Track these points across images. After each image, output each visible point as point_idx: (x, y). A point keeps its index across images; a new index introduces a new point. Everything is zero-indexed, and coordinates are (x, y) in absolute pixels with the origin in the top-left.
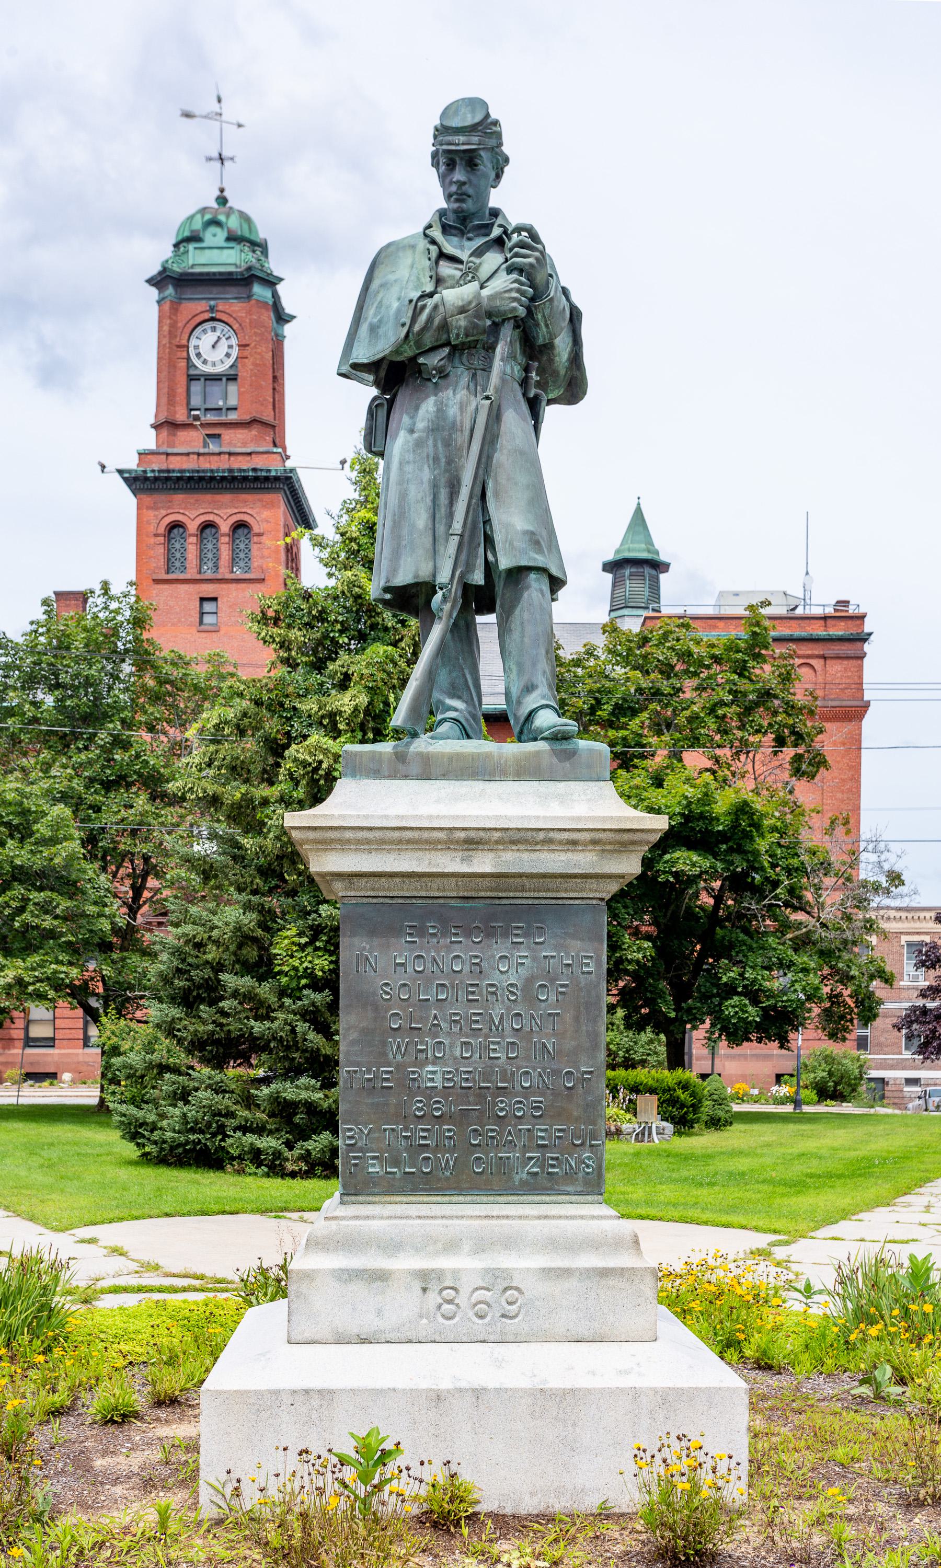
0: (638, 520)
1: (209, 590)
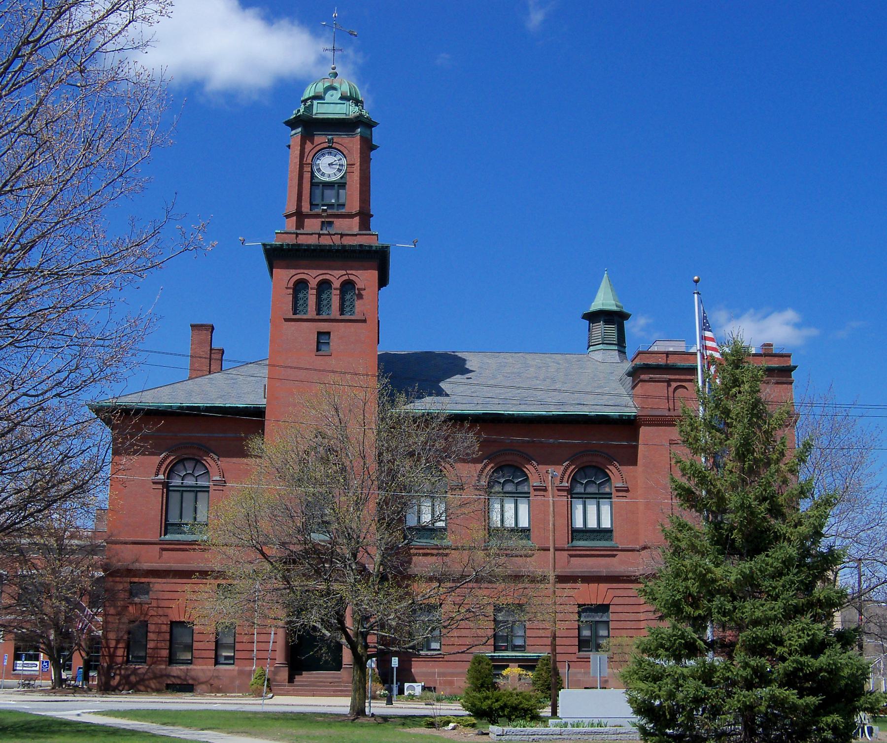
1: (324, 327)
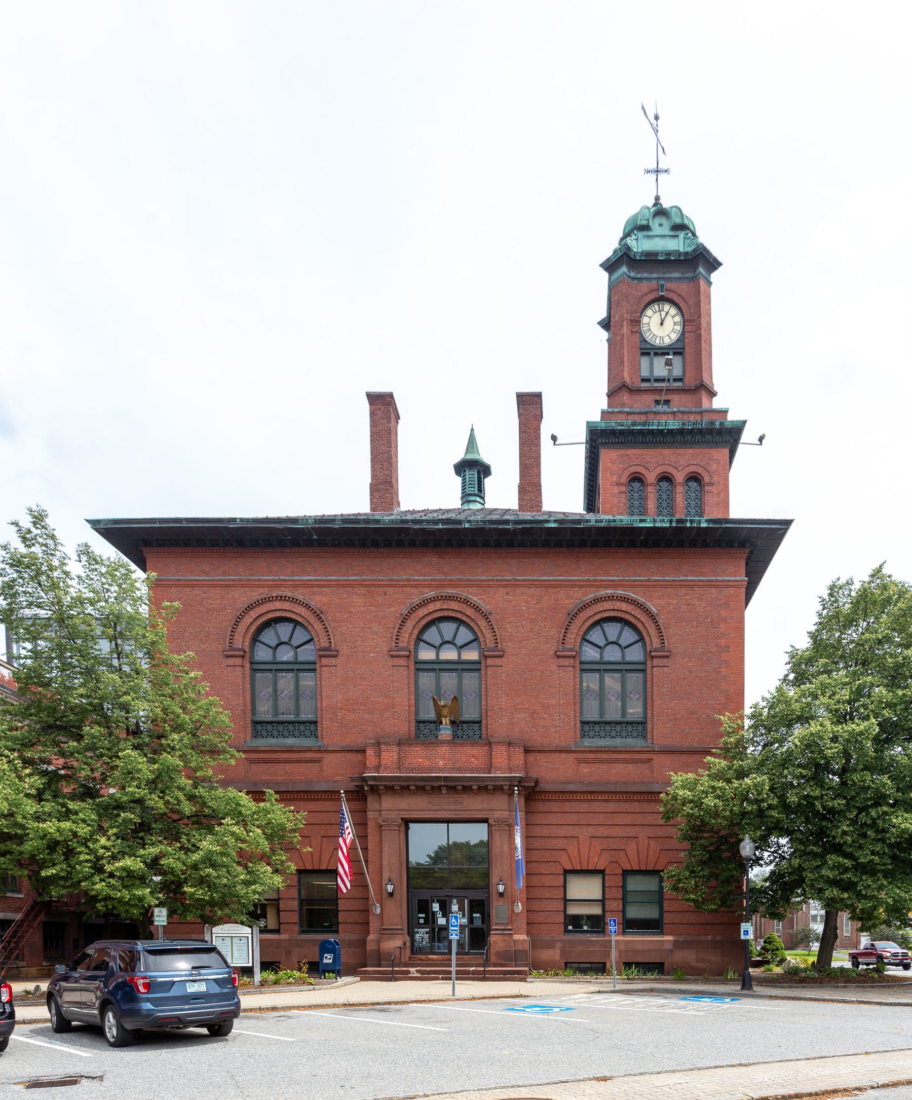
0: (472, 443)
